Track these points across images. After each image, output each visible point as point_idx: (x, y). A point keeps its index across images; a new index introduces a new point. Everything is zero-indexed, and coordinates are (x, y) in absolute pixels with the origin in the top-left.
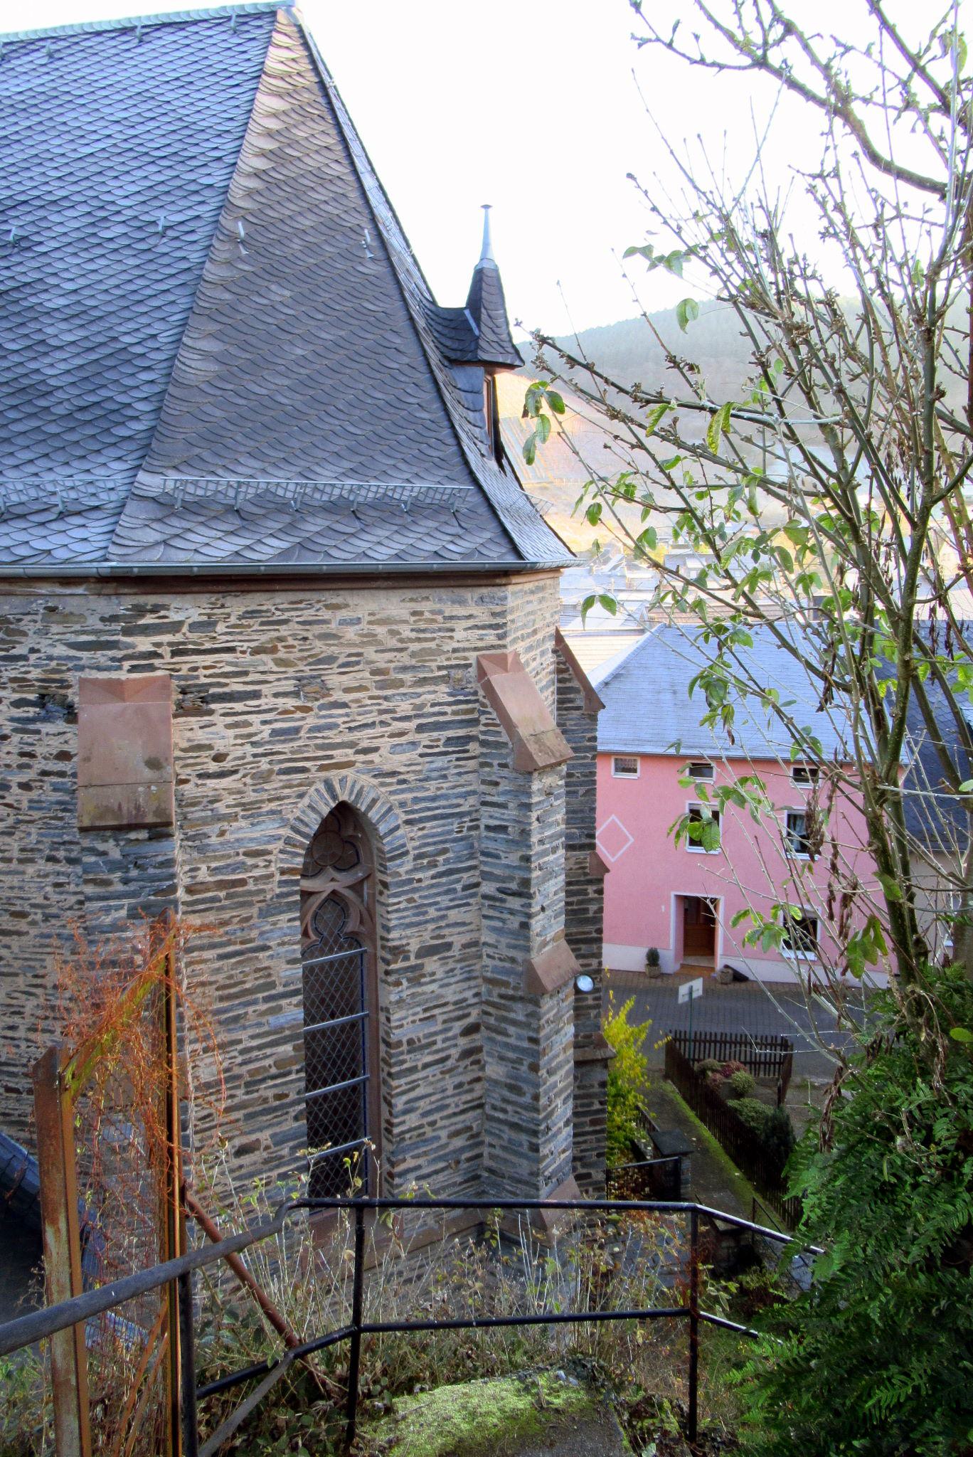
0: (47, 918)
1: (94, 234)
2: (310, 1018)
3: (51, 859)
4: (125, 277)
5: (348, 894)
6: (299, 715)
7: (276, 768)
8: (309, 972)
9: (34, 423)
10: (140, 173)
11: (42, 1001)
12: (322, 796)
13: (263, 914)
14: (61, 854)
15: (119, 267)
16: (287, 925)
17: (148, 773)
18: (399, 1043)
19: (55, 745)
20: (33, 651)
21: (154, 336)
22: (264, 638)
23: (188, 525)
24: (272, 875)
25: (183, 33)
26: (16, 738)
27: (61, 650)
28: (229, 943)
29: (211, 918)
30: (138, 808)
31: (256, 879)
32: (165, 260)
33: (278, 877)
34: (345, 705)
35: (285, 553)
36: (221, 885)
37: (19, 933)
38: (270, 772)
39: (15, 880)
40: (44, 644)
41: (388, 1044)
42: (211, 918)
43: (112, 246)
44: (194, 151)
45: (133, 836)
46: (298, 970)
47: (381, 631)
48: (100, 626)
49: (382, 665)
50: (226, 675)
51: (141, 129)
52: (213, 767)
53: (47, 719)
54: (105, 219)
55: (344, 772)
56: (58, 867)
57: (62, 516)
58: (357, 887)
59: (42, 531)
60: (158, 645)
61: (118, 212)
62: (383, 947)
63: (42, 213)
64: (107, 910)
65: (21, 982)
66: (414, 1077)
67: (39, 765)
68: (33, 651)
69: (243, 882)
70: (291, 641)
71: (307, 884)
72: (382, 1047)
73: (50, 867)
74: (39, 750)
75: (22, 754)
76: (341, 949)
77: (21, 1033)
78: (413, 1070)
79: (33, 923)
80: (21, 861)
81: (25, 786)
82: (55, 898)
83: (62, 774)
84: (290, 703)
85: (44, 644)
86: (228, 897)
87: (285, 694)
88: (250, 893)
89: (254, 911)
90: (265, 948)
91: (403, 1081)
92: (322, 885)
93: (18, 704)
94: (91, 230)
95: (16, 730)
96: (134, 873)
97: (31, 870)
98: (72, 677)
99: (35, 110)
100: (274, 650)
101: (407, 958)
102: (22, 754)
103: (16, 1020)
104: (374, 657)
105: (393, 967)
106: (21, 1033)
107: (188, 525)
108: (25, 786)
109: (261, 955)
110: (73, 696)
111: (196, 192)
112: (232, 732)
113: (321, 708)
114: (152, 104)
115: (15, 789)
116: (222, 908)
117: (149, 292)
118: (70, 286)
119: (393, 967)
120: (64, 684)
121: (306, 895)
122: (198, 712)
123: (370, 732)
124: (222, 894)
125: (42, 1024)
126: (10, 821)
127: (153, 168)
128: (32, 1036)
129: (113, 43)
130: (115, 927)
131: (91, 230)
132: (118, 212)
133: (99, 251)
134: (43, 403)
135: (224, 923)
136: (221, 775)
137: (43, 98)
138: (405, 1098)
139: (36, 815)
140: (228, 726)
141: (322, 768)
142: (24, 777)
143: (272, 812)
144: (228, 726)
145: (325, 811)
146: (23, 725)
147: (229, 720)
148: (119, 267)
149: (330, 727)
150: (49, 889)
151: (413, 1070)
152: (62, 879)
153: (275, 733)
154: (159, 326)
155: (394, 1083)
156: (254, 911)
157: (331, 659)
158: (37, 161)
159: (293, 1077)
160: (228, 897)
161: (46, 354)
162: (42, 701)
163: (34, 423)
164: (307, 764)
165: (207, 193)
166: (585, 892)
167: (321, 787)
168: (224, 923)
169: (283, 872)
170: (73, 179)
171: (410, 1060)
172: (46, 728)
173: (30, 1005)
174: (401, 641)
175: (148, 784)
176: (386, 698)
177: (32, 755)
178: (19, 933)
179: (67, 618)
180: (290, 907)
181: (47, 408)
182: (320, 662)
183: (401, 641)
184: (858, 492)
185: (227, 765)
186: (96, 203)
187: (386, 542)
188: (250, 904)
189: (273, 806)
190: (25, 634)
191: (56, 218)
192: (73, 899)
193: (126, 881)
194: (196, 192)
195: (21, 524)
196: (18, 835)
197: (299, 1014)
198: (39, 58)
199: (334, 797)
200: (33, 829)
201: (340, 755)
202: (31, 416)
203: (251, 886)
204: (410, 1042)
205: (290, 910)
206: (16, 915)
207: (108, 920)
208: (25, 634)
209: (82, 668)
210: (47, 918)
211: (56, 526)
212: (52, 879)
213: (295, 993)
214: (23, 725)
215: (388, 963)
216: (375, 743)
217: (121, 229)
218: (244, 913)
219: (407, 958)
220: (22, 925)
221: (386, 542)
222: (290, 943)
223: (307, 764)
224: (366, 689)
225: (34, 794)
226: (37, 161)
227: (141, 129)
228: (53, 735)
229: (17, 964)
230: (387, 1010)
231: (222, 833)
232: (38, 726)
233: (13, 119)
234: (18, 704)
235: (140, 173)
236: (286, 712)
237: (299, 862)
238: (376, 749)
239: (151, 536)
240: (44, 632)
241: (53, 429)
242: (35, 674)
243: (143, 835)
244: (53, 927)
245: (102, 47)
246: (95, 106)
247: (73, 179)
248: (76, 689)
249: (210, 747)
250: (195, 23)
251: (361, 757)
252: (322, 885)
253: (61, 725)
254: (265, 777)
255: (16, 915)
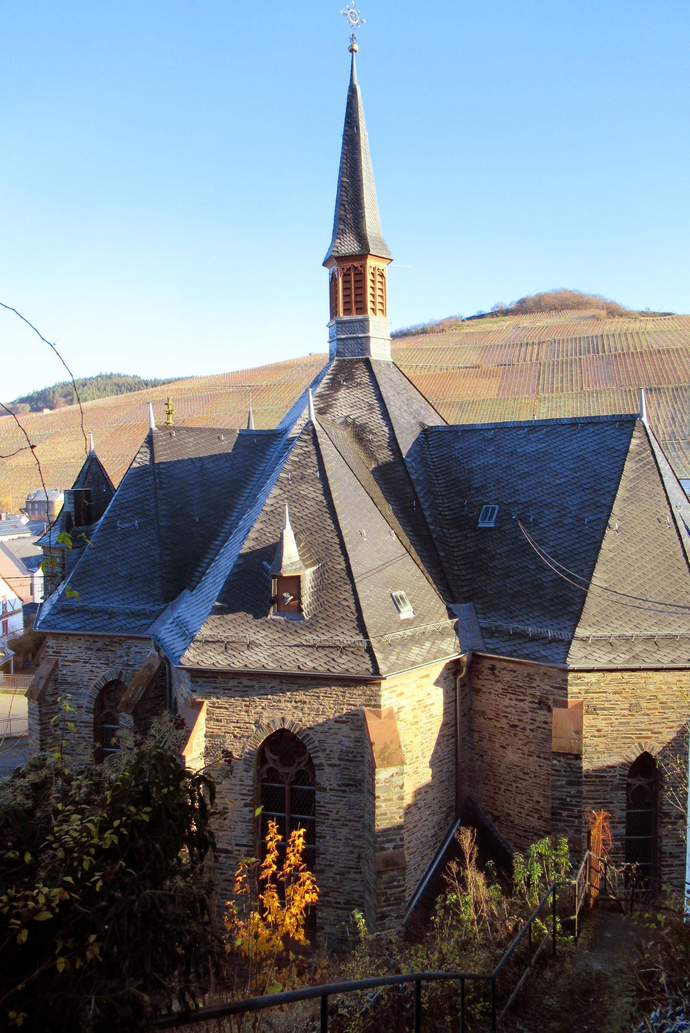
0: (535, 777)
1: (561, 522)
2: (628, 834)
3: (538, 757)
4: (572, 542)
5: (647, 787)
6: (629, 717)
7: (620, 736)
8: (628, 815)
9: (539, 601)
10: (578, 495)
11: (531, 805)
12: (637, 749)
13: (613, 790)
14: (542, 756)
15: (570, 538)
16: (621, 795)
17: (575, 736)
18: (665, 853)
19: (543, 718)
20: (538, 686)
21: (582, 570)
22: (617, 688)
23: (594, 649)
24: (616, 776)
25: (596, 428)
26: (530, 714)
27: (548, 688)
28: (599, 799)
29: (592, 788)
30: (571, 747)
31: (610, 776)
32: (587, 537)
33: (618, 777)
34: (648, 715)
35: (627, 661)
36: (597, 777)
37: (525, 780)
38: (618, 737)
39: (525, 761)
40: (542, 685)
41: (661, 852)
42: (592, 788)
43: (568, 528)
44: (599, 487)
45: (569, 757)
46: (624, 814)
47: (664, 687)
48: (561, 682)
49: (664, 700)
50: (603, 701)
51: (579, 474)
52: (596, 734)
53: (541, 709)
54: (565, 515)
55: (647, 740)
56: (540, 760)
57: (550, 642)
58: (650, 785)
59: (543, 647)
60: (580, 690)
61: (570, 513)
62: (661, 812)
63: (541, 509)
64: (559, 780)
65: (525, 797)
66: (672, 869)
67: (538, 724)
68: (538, 686)
69: (605, 777)
70: (627, 690)
71: (630, 780)
72: (658, 853)
73: (538, 759)
74: (537, 719)
75: (532, 719)
76: (642, 808)
77: (523, 815)
78: (671, 865)
79: (530, 777)
80: (529, 755)
81: (532, 730)
82: (538, 770)
83: (544, 728)
84: (626, 712)
85: (542, 685)
86: (599, 781)
87: (625, 709)
88: (607, 781)
89: (609, 788)
90: (612, 803)
91: (667, 869)
92: (636, 782)
93: (531, 702)
94: (560, 519)
95: (530, 711)
96: (569, 769)
97: (531, 759)
98: (551, 697)
99: (539, 460)
100: (621, 693)
101: (670, 818)
102: (532, 719)
103: (522, 810)
104: (661, 697)
105: (664, 820)
106: (523, 815)
107: (594, 649)
108: (532, 730)
109: (610, 805)
110: (551, 703)
111: (599, 507)
112: (604, 722)
113: (639, 715)
114: (583, 462)
115: (528, 731)
116: (596, 785)
117: (581, 550)
118: (551, 544)
119: (664, 820)
120: (548, 699)
121: (629, 784)
122: (592, 714)
123: (659, 726)
124: (597, 780)
125: (531, 814)
126: (526, 741)
127: (583, 494)
128: (527, 817)
129: (568, 430)
130: (562, 786)
131: (560, 519)
132: (570, 513)
133: (562, 529)
134: (542, 593)
135: (597, 791)
136: (600, 737)
137: (541, 455)
138: (667, 876)
139: (534, 740)
140: (602, 719)
141: (638, 738)
142: (531, 727)
143: (617, 752)
144: (602, 719)
145: (638, 755)
146: (533, 710)
147: (603, 717)
148: (570, 538)
149: (641, 723)
150: (537, 767)
151: (671, 865)
152: (541, 764)
153: (620, 723)
154: (584, 566)
155: (663, 869)
156: (609, 788)
157: (643, 697)
158: (540, 485)
159: (620, 855)
160: (599, 781)
161: (543, 572)
162: (540, 703)
163: (539, 601)
164: (632, 736)
165: (604, 508)
166: (574, 822)
167: (637, 744)
168: (597, 791)
169: (621, 775)
170: (553, 495)
171: (670, 861)
172: (540, 712)
173: (527, 806)
174: (673, 691)
175: (575, 739)
176: (665, 713)
177: (534, 720)
178: (525, 780)
179: (550, 677)
180: (623, 789)
181: (543, 595)
182: (639, 698)
183: (673, 691)
184: (583, 844)
185: (603, 733)
186: (555, 473)
187: (667, 655)
188: (607, 785)
189: (618, 750)
190: (535, 680)
191: (546, 512)
192: (545, 772)
193: (565, 771)
194: (599, 507)
195: (536, 643)
196: (528, 746)
197: (624, 831)
198: (540, 434)
199: (642, 750)
200: (533, 745)
201: (645, 734)
202: (538, 597)
203: (608, 779)
204: (670, 853)
205: (622, 790)
206: (525, 773)
207: (559, 783)
208: (535, 680)
209: (554, 695)
210: (535, 777)
211: (548, 646)
212: (538, 763)
213: (622, 822)
214: (533, 710)
215: (662, 818)
216: (660, 730)
217: (570, 520)
218: (605, 788)
219: (670, 818)
220: (527, 777)
221: (667, 655)
222: (621, 803)
223: (632, 736)
224: (657, 709)
225: (534, 734)
226: (540, 485)
227: (579, 474)
228: (542, 715)
229: (524, 790)
230: (660, 838)
231: (598, 758)
232: (538, 711)
233: (530, 464)
234: (531, 702)
235: (578, 495)
236: (624, 716)
237: (626, 772)
238: (660, 733)
239: (581, 654)
240: (542, 681)
241: (546, 604)
242: (538, 694)
243: (572, 757)
244: (538, 780)
245: (564, 432)
246: (561, 461)
247: (553, 495)
248: (552, 701)
249: (596, 726)
250: (602, 423)
251: (654, 735)
252: (636, 782)
253: (545, 712)
254: (616, 739)
255: (525, 773)
